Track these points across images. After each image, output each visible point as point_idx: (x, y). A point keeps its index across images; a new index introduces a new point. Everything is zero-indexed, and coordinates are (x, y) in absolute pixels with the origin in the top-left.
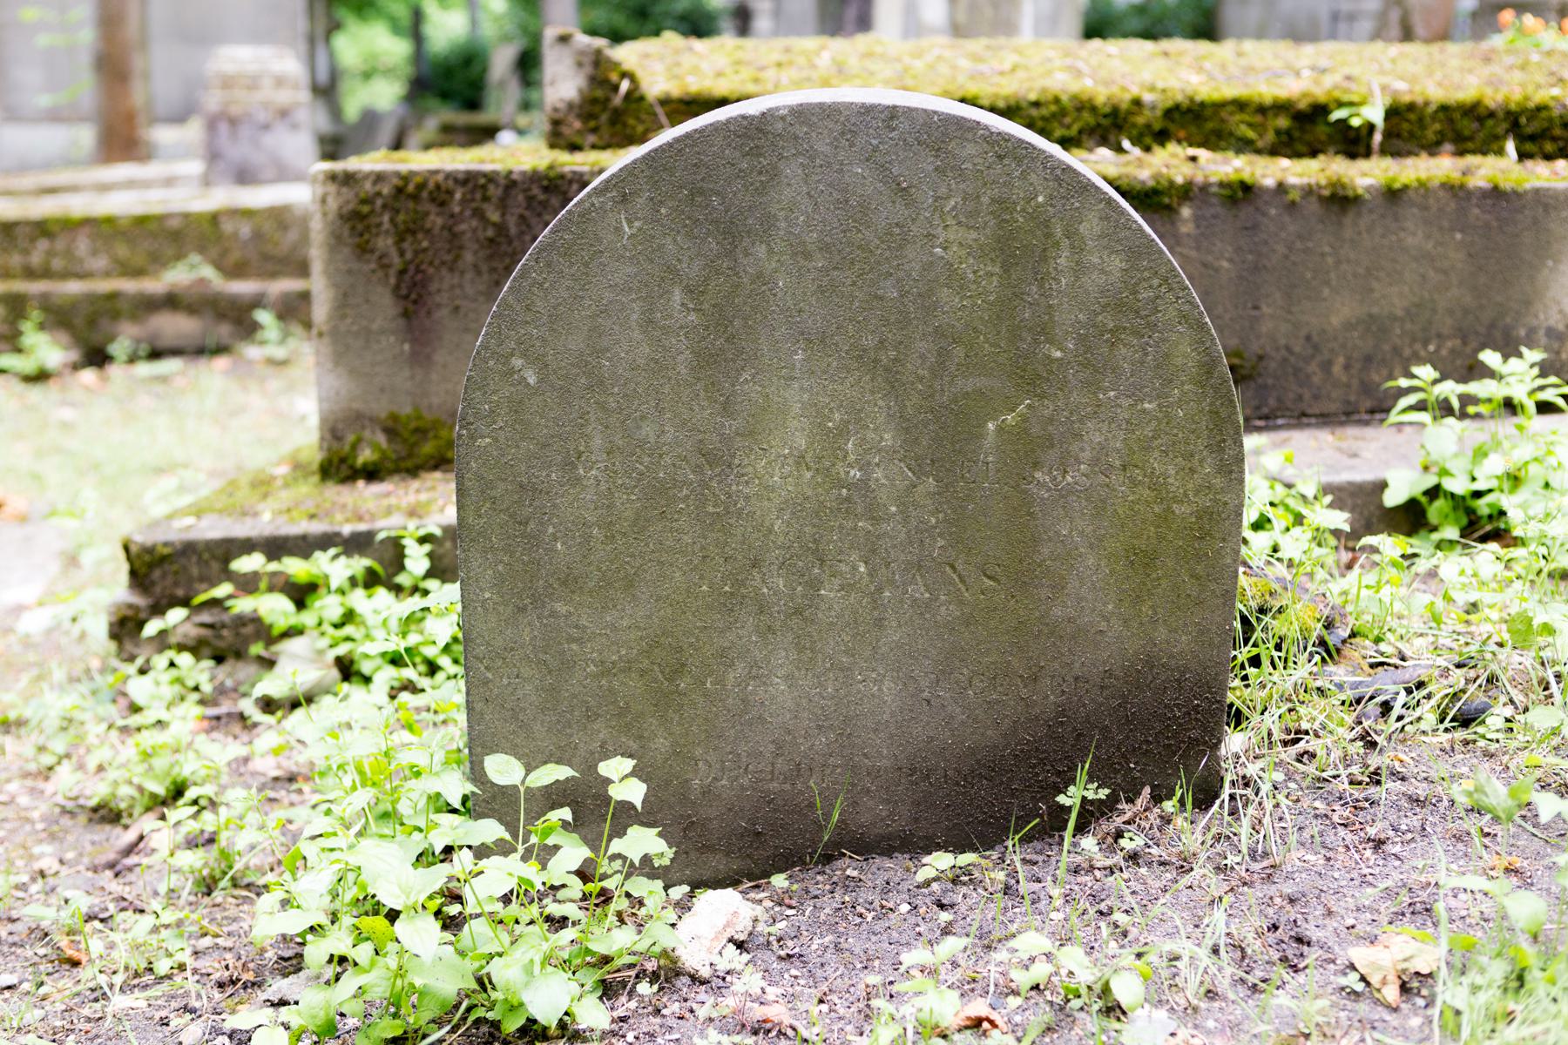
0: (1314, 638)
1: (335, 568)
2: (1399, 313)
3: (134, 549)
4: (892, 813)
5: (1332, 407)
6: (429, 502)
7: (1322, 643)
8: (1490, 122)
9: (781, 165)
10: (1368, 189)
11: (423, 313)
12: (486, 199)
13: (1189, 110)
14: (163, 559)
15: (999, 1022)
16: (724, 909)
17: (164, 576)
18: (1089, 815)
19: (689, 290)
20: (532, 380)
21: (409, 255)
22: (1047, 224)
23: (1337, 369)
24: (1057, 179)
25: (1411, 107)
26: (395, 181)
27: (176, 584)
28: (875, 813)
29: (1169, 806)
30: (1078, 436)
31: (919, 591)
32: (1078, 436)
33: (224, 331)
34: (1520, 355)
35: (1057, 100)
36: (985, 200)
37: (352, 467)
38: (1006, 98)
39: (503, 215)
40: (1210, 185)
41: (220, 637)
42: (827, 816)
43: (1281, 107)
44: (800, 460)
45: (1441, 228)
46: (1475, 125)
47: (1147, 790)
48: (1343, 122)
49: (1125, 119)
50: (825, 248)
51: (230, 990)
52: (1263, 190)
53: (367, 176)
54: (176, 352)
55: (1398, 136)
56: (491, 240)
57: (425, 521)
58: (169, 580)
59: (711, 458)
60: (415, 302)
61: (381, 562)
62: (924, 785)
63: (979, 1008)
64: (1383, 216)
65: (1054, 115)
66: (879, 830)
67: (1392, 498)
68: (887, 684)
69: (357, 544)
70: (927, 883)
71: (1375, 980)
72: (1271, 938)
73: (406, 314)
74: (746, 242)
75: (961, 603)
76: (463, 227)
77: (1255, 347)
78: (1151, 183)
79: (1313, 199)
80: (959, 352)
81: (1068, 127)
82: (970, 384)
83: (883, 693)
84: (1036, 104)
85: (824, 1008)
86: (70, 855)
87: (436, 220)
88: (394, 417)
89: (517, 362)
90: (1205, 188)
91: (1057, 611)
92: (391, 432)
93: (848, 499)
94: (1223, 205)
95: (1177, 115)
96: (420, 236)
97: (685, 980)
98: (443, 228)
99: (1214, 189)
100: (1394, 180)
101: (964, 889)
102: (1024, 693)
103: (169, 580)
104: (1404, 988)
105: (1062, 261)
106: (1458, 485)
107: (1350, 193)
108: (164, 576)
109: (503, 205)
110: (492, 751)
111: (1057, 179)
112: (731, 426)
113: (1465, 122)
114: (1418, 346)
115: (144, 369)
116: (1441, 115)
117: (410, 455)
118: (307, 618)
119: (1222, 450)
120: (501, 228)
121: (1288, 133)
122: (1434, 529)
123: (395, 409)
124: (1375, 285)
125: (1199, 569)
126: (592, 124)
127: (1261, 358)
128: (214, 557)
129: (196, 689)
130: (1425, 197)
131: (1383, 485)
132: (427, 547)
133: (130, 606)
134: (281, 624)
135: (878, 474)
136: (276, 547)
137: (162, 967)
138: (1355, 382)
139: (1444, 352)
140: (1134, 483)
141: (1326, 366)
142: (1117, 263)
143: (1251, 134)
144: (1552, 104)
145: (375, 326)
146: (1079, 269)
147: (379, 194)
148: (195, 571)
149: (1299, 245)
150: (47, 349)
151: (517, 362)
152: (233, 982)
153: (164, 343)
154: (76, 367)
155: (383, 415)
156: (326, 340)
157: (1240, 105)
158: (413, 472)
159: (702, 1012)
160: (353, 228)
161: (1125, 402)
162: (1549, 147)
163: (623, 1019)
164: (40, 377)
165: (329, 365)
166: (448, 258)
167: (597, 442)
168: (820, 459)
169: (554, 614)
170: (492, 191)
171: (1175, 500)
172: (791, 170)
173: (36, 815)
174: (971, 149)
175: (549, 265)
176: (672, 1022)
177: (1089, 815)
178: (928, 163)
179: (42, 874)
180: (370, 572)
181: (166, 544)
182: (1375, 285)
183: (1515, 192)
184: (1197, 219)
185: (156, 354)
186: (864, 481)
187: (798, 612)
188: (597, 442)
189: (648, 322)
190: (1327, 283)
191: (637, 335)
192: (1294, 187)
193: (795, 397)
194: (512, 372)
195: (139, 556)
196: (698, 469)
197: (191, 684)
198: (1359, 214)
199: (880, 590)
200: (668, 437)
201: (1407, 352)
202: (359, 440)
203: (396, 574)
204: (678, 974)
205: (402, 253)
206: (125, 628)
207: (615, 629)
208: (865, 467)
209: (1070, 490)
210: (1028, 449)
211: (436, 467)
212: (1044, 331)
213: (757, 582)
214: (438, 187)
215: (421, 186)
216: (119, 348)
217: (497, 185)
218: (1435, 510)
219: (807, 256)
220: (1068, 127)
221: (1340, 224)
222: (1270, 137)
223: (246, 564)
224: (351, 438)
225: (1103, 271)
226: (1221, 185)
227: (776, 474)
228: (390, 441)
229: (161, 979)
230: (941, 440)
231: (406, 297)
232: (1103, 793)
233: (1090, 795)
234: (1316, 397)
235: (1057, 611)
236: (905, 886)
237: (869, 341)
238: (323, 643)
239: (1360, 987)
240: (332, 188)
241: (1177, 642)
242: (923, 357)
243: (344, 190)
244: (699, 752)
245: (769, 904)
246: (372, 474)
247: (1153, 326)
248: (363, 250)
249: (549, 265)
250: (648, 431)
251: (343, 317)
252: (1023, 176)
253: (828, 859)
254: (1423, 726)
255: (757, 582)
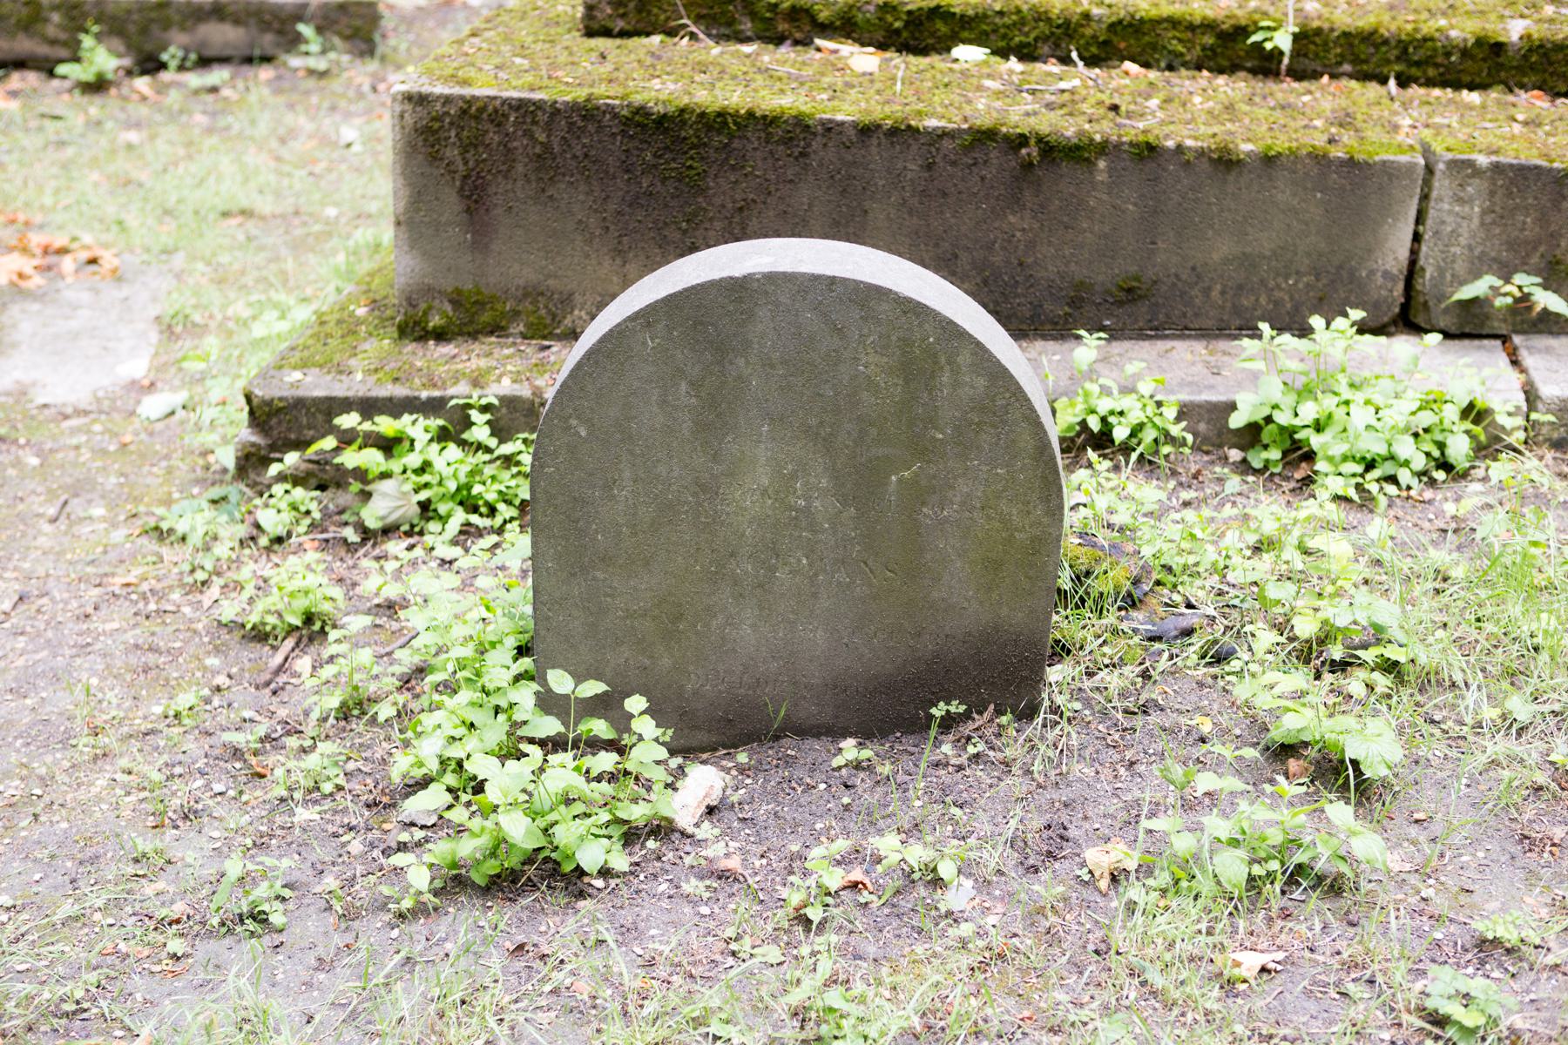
0: (1123, 592)
1: (418, 428)
2: (1268, 253)
3: (255, 401)
4: (820, 713)
5: (1209, 323)
6: (490, 370)
7: (1130, 595)
8: (1384, 49)
9: (756, 309)
10: (1248, 154)
11: (482, 211)
12: (534, 122)
13: (1130, 25)
14: (279, 410)
15: (869, 885)
16: (705, 780)
17: (280, 422)
18: (948, 723)
19: (691, 384)
20: (583, 434)
21: (471, 164)
22: (935, 355)
23: (1215, 294)
24: (943, 328)
25: (1318, 32)
26: (461, 104)
27: (289, 429)
28: (810, 711)
29: (1004, 720)
30: (952, 487)
31: (841, 576)
32: (952, 487)
33: (268, 39)
34: (1346, 315)
35: (1019, 11)
36: (894, 338)
37: (424, 329)
38: (975, 7)
39: (548, 136)
40: (1123, 144)
41: (324, 471)
42: (777, 712)
43: (1208, 26)
44: (764, 492)
45: (1305, 189)
46: (1372, 50)
47: (992, 707)
48: (1258, 46)
49: (1075, 31)
50: (784, 362)
51: (375, 810)
52: (1166, 150)
53: (439, 97)
54: (223, 60)
55: (1305, 55)
56: (539, 156)
57: (486, 392)
58: (284, 427)
59: (704, 488)
60: (476, 202)
61: (450, 422)
62: (843, 696)
63: (857, 874)
64: (1260, 177)
65: (1014, 24)
66: (813, 721)
67: (1237, 421)
68: (820, 633)
69: (432, 407)
70: (840, 768)
71: (1097, 874)
72: (1046, 834)
73: (468, 210)
74: (731, 355)
75: (870, 585)
76: (515, 144)
77: (1150, 273)
78: (1075, 141)
79: (1205, 160)
80: (874, 431)
81: (1027, 35)
82: (880, 452)
83: (819, 638)
84: (1001, 13)
85: (764, 861)
86: (234, 670)
87: (493, 137)
88: (458, 291)
89: (574, 422)
90: (1118, 146)
91: (935, 594)
92: (456, 303)
93: (796, 518)
94: (1132, 160)
95: (1119, 28)
96: (481, 149)
97: (677, 835)
98: (499, 143)
99: (1126, 147)
100: (1270, 148)
101: (862, 775)
102: (911, 643)
103: (284, 427)
104: (1114, 879)
105: (945, 379)
106: (1283, 418)
107: (1234, 158)
108: (280, 422)
109: (549, 128)
110: (534, 544)
111: (943, 328)
112: (717, 469)
113: (1363, 47)
114: (1280, 280)
115: (194, 79)
116: (1342, 41)
117: (471, 322)
118: (395, 466)
119: (1048, 501)
120: (547, 147)
121: (1212, 48)
122: (1266, 447)
123: (459, 285)
124: (1250, 229)
125: (1031, 573)
126: (621, 11)
127: (1155, 282)
128: (319, 410)
129: (308, 513)
130: (1294, 163)
131: (1232, 407)
132: (488, 416)
133: (253, 445)
134: (375, 471)
135: (817, 504)
136: (369, 407)
137: (327, 788)
138: (1229, 305)
139: (1301, 286)
140: (989, 518)
141: (1207, 292)
142: (981, 382)
143: (1180, 48)
144: (1437, 35)
145: (443, 220)
146: (956, 384)
147: (447, 113)
148: (305, 421)
149: (1190, 195)
150: (101, 58)
151: (574, 422)
152: (376, 805)
153: (209, 53)
154: (129, 73)
155: (450, 290)
156: (403, 228)
157: (1174, 22)
158: (474, 335)
159: (688, 860)
160: (425, 140)
161: (984, 468)
162: (1431, 72)
163: (637, 864)
164: (97, 86)
165: (406, 248)
166: (504, 168)
167: (627, 474)
168: (777, 492)
169: (594, 578)
170: (542, 117)
171: (1016, 530)
172: (763, 313)
173: (200, 626)
174: (885, 306)
175: (597, 362)
176: (668, 867)
177: (948, 723)
178: (856, 314)
179: (218, 689)
180: (443, 429)
181: (281, 399)
182: (1250, 229)
183: (1366, 163)
184: (1110, 170)
185: (205, 62)
186: (808, 507)
187: (760, 586)
188: (627, 474)
189: (663, 402)
190: (1211, 226)
191: (655, 409)
192: (1190, 148)
193: (762, 453)
194: (569, 428)
195: (260, 407)
196: (695, 495)
197: (303, 509)
198: (1240, 173)
199: (816, 575)
200: (675, 474)
201: (1272, 284)
202: (430, 308)
203: (463, 432)
204: (673, 830)
205: (466, 163)
206: (251, 463)
207: (635, 589)
208: (808, 499)
209: (946, 520)
210: (918, 494)
211: (491, 333)
212: (932, 422)
213: (734, 566)
214: (496, 111)
215: (482, 110)
216: (170, 55)
217: (545, 112)
218: (1267, 434)
219: (772, 366)
220: (1027, 35)
221: (1225, 181)
222: (1198, 51)
223: (348, 421)
224: (423, 306)
225: (972, 387)
226: (1131, 144)
227: (749, 498)
228: (454, 310)
229: (325, 797)
230: (860, 485)
231: (469, 197)
232: (962, 708)
233: (953, 709)
234: (1196, 315)
235: (935, 594)
236: (824, 767)
237: (813, 422)
238: (408, 487)
239: (1087, 878)
240: (408, 107)
241: (1015, 616)
242: (849, 433)
243: (419, 109)
244: (691, 668)
245: (734, 772)
246: (441, 336)
247: (1005, 422)
248: (434, 158)
249: (597, 362)
250: (662, 469)
251: (418, 210)
252: (920, 325)
253: (777, 738)
254: (1189, 663)
255: (734, 566)
